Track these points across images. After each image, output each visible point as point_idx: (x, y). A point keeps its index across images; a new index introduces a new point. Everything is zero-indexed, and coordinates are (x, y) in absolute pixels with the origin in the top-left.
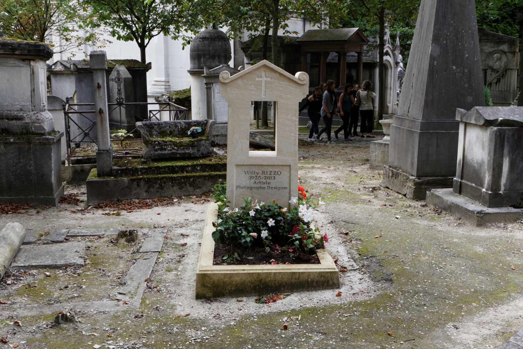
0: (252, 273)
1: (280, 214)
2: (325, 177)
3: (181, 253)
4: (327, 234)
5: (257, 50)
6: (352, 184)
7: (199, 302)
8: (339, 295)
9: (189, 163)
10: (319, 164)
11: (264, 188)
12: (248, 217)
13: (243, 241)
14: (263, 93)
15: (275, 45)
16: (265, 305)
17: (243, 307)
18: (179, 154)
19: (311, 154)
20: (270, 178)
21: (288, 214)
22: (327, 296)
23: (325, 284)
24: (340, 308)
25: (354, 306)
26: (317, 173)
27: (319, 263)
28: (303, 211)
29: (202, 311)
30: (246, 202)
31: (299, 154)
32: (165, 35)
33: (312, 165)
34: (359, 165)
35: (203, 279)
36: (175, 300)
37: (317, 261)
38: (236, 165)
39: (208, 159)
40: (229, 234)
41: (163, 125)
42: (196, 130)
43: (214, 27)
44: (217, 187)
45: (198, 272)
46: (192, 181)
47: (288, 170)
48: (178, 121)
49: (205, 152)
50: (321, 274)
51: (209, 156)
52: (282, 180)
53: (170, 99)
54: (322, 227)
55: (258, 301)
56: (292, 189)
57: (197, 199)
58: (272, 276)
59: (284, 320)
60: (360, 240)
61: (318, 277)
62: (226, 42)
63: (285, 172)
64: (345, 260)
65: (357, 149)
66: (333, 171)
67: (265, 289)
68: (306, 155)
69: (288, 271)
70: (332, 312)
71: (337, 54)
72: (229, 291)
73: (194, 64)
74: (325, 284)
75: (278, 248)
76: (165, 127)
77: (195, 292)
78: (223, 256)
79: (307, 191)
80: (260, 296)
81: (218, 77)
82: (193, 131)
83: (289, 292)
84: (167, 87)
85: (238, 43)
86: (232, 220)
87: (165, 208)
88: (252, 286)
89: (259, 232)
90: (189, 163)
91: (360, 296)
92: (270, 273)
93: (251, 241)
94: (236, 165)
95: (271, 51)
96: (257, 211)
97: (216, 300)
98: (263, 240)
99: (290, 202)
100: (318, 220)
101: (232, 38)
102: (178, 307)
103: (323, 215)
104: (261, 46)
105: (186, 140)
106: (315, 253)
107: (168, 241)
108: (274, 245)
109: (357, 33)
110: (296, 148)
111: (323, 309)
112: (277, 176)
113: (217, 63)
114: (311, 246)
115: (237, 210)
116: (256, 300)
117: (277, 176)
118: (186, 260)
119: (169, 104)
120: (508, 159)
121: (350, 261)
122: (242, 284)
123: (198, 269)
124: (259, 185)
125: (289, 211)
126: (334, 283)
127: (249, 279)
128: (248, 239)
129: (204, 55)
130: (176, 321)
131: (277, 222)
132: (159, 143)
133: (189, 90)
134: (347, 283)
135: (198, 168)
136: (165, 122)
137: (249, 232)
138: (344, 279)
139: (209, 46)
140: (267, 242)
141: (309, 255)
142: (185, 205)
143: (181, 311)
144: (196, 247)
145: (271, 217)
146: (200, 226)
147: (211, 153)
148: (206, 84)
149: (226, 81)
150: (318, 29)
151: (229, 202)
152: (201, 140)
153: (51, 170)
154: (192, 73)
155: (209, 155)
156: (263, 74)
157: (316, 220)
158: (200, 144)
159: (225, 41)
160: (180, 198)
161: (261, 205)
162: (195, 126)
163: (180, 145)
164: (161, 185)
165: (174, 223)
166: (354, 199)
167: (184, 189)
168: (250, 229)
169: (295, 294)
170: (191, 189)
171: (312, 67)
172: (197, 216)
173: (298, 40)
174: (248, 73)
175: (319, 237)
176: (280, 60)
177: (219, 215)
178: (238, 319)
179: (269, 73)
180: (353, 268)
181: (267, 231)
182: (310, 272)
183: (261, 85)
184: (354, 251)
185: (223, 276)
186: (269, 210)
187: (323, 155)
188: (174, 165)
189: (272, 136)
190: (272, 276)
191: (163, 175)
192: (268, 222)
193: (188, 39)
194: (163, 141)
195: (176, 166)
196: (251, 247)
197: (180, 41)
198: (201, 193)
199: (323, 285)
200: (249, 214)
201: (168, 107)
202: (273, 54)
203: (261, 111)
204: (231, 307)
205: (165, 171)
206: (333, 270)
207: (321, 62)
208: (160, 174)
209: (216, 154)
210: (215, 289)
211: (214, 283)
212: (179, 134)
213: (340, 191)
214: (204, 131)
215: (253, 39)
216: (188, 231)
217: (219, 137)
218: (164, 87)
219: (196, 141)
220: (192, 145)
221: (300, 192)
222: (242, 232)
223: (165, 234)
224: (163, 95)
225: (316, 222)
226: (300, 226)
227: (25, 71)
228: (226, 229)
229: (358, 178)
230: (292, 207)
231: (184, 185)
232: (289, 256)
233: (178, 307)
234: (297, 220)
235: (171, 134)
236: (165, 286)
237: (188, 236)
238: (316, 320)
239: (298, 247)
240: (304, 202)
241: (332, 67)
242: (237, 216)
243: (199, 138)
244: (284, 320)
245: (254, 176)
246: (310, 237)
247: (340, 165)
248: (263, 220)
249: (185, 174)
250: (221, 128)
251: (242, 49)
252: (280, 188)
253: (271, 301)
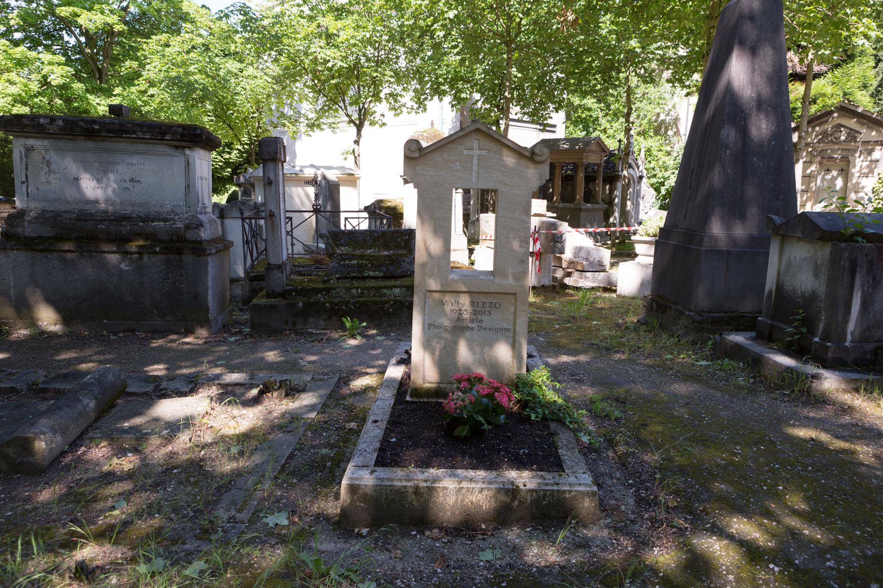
14: (474, 175)
47: (513, 301)
110: (578, 245)
120: (859, 294)
153: (207, 289)
183: (472, 163)
227: (178, 161)
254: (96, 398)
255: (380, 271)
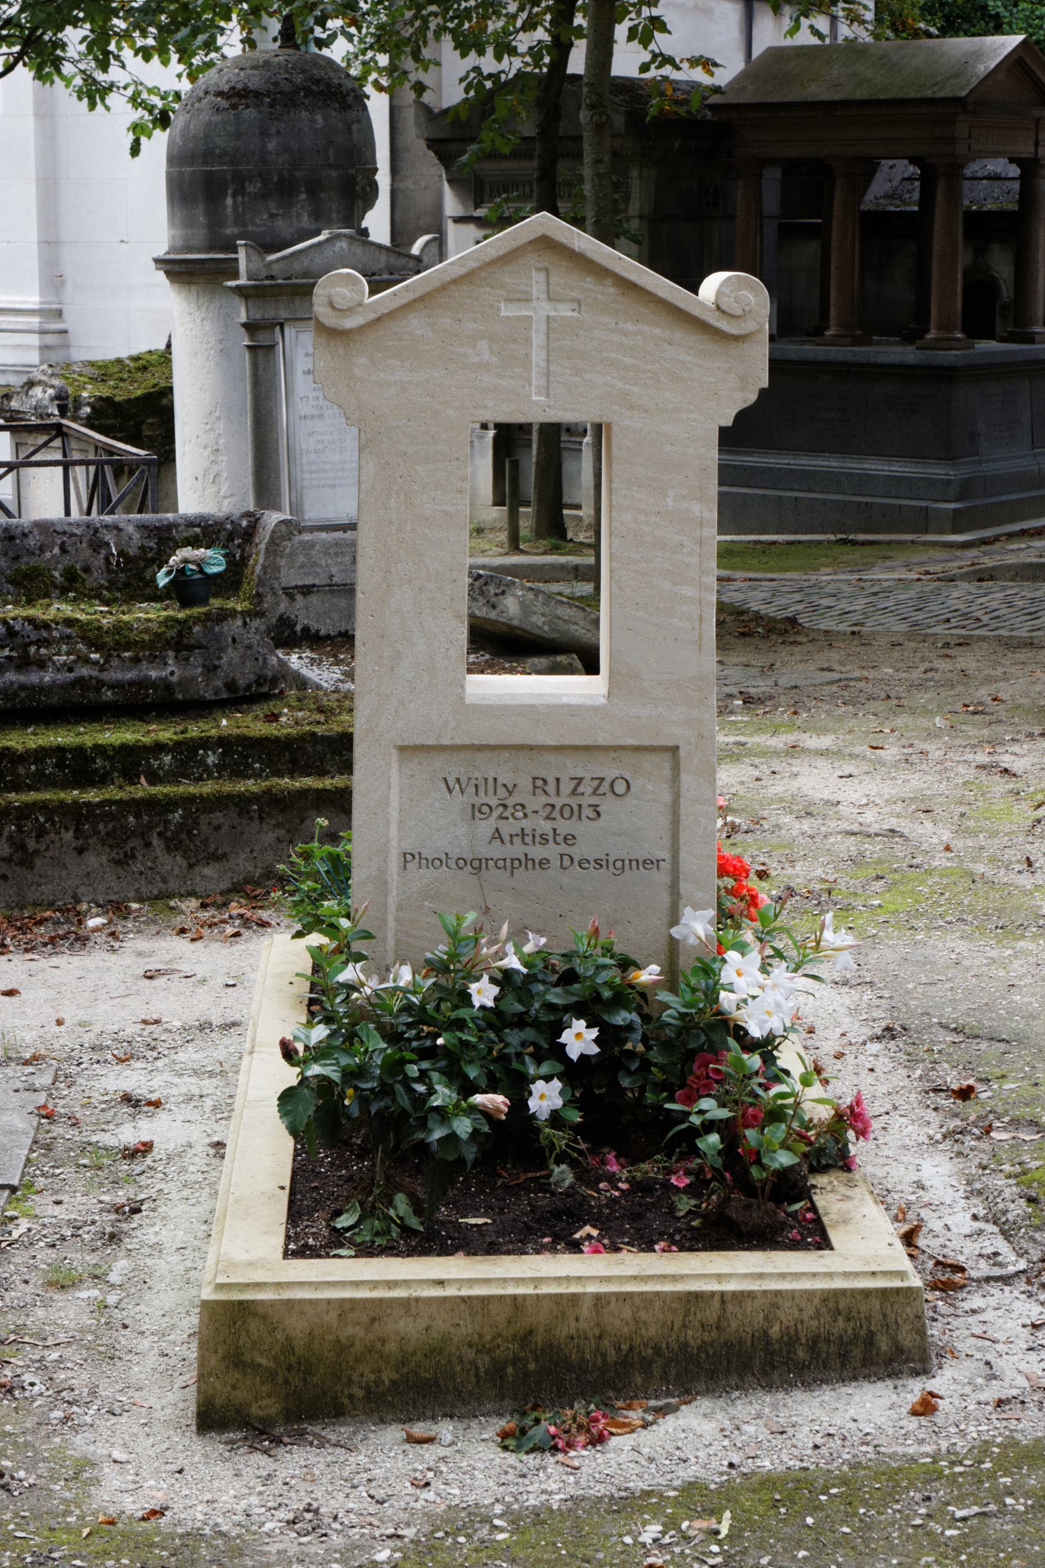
0: (485, 1301)
1: (627, 995)
2: (853, 797)
3: (121, 1196)
4: (866, 1096)
5: (506, 150)
6: (993, 835)
7: (215, 1446)
8: (926, 1407)
9: (166, 733)
10: (823, 731)
11: (544, 863)
12: (463, 1013)
13: (438, 1134)
14: (537, 379)
15: (599, 128)
16: (550, 1460)
17: (437, 1473)
18: (112, 686)
19: (785, 681)
20: (574, 813)
21: (664, 996)
22: (865, 1414)
23: (857, 1352)
24: (933, 1475)
25: (1002, 1465)
26: (816, 780)
27: (824, 1243)
28: (740, 982)
29: (226, 1488)
30: (454, 935)
31: (722, 680)
32: (40, 76)
33: (790, 738)
34: (1030, 735)
35: (234, 1330)
36: (90, 1435)
37: (815, 1236)
38: (402, 749)
39: (260, 710)
40: (363, 1100)
41: (31, 542)
42: (200, 564)
43: (288, 36)
44: (307, 856)
45: (208, 1294)
46: (181, 826)
48: (108, 518)
49: (244, 677)
50: (833, 1302)
51: (266, 697)
52: (632, 821)
53: (65, 403)
54: (839, 1056)
55: (513, 1440)
56: (684, 867)
57: (205, 915)
58: (585, 1310)
59: (646, 1538)
60: (1033, 1124)
61: (817, 1315)
62: (352, 114)
63: (650, 785)
64: (956, 1228)
65: (1022, 656)
66: (895, 765)
67: (549, 1381)
68: (760, 687)
69: (668, 1287)
70: (890, 1496)
71: (913, 170)
72: (367, 1389)
73: (188, 223)
74: (857, 1352)
75: (614, 1168)
76: (42, 549)
77: (192, 1393)
78: (338, 1213)
79: (762, 875)
80: (524, 1414)
81: (306, 291)
82: (181, 571)
83: (669, 1394)
84: (50, 339)
85: (409, 115)
86: (380, 1028)
87: (43, 963)
88: (484, 1362)
89: (518, 1089)
90: (166, 733)
91: (1033, 1411)
92: (575, 1299)
93: (475, 1133)
94: (402, 749)
95: (579, 155)
96: (505, 979)
97: (302, 1433)
98: (538, 1131)
99: (675, 932)
100: (819, 1024)
101: (380, 88)
102: (107, 1469)
103: (847, 998)
104: (529, 130)
105: (147, 614)
106: (804, 1193)
107: (58, 1130)
108: (594, 1151)
109: (1016, 60)
111: (844, 1481)
112: (607, 804)
113: (305, 221)
114: (784, 1159)
115: (405, 975)
116: (505, 1435)
117: (607, 804)
118: (146, 1231)
119: (59, 431)
121: (980, 1232)
122: (433, 1351)
123: (208, 1276)
124: (517, 850)
125: (671, 980)
126: (899, 1349)
127: (467, 1329)
128: (463, 1126)
129: (240, 182)
130: (98, 1544)
131: (609, 1037)
132: (11, 633)
133: (165, 357)
134: (964, 1346)
135: (211, 759)
136: (44, 527)
137: (468, 1088)
138: (950, 1326)
139: (264, 134)
140: (561, 1139)
141: (771, 1206)
142: (141, 944)
143: (119, 1494)
144: (198, 1160)
145: (581, 1010)
146: (221, 1054)
147: (274, 682)
148: (250, 327)
149: (350, 323)
150: (815, 41)
151: (367, 936)
152: (225, 615)
154: (178, 270)
155: (262, 691)
156: (537, 284)
157: (808, 1021)
158: (217, 638)
159: (345, 107)
160: (118, 909)
161: (528, 948)
162: (194, 542)
163: (115, 642)
164: (23, 847)
165: (88, 1039)
166: (1000, 912)
167: (137, 866)
168: (473, 1072)
169: (704, 1404)
170: (172, 863)
171: (788, 233)
172: (205, 1004)
173: (715, 99)
174: (457, 281)
175: (824, 1113)
176: (627, 200)
177: (320, 998)
178: (409, 1533)
179: (564, 278)
180: (997, 1272)
181: (557, 1084)
182: (777, 1293)
183: (528, 341)
184: (1000, 1182)
185: (334, 1314)
186: (569, 978)
187: (844, 683)
188: (88, 740)
189: (587, 588)
190: (585, 1310)
191: (33, 796)
192: (567, 1037)
193: (160, 104)
194: (31, 620)
195: (96, 747)
196: (476, 1163)
197: (121, 112)
198: (224, 885)
199: (844, 1357)
200: (465, 998)
201: (57, 443)
202: (587, 172)
203: (531, 459)
204: (378, 1473)
205: (40, 773)
206: (897, 1283)
207: (837, 213)
208: (17, 788)
209: (302, 683)
210: (296, 1381)
211: (288, 1347)
212: (112, 586)
213: (929, 872)
214: (236, 567)
215: (486, 96)
216: (158, 1081)
217: (314, 599)
218: (34, 340)
219: (198, 620)
220: (177, 641)
221: (729, 882)
222: (431, 1091)
223: (41, 1098)
224: (31, 384)
225: (811, 1031)
226: (729, 1056)
228: (351, 1075)
229: (1024, 806)
230: (686, 962)
231: (135, 842)
232: (672, 1208)
233: (107, 1469)
234: (712, 1027)
235: (72, 584)
236: (41, 1365)
237: (157, 1104)
238: (809, 1537)
239: (719, 1163)
240: (748, 936)
241: (892, 235)
242: (408, 1008)
243: (216, 603)
244: (646, 1538)
245: (493, 802)
246: (776, 1115)
247: (932, 734)
248: (536, 1024)
249: (143, 789)
250: (328, 549)
251: (433, 144)
252: (621, 866)
253: (581, 1439)
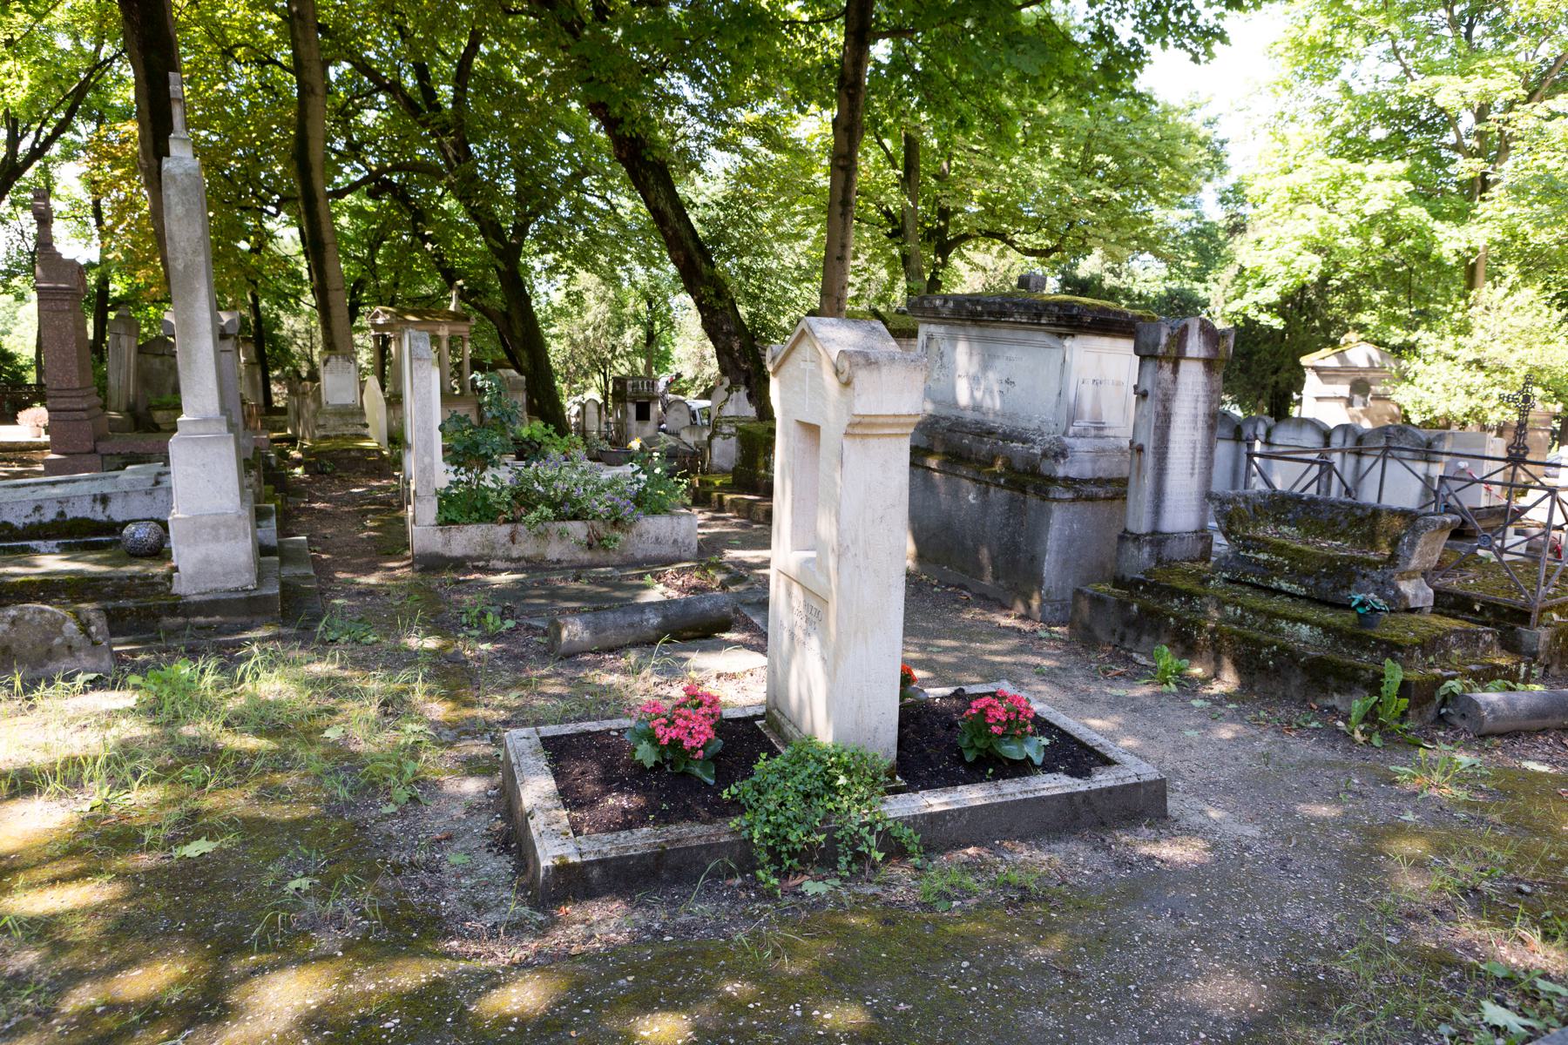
227: (1056, 355)
254: (665, 617)
255: (1301, 584)
